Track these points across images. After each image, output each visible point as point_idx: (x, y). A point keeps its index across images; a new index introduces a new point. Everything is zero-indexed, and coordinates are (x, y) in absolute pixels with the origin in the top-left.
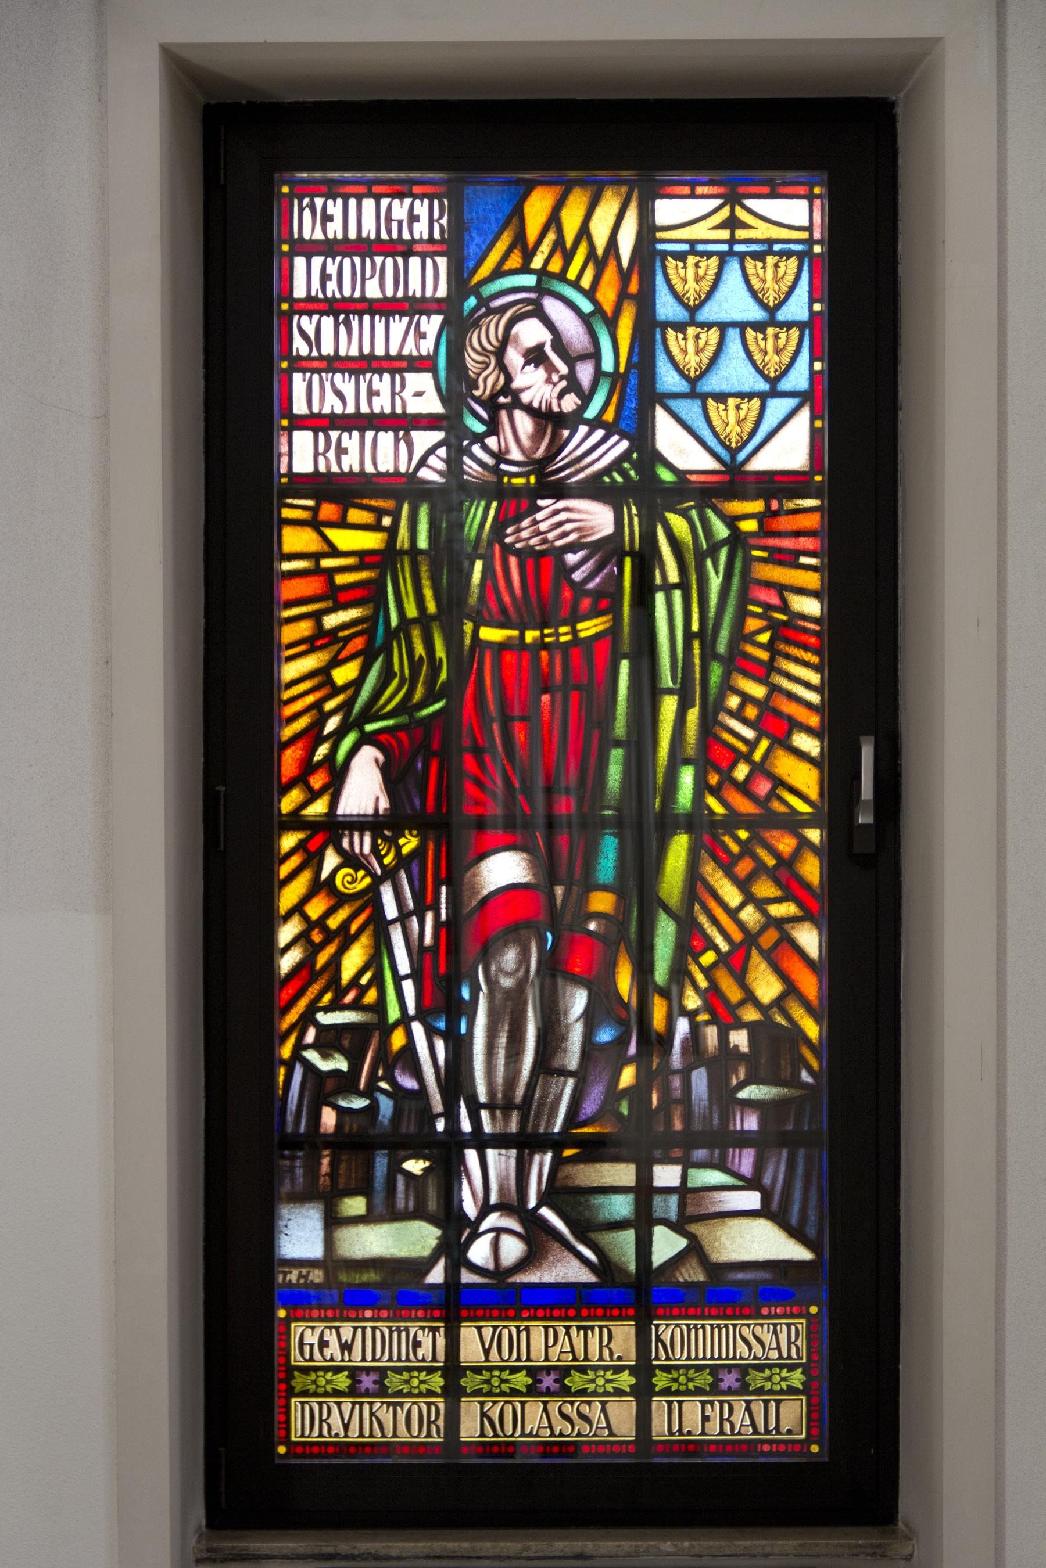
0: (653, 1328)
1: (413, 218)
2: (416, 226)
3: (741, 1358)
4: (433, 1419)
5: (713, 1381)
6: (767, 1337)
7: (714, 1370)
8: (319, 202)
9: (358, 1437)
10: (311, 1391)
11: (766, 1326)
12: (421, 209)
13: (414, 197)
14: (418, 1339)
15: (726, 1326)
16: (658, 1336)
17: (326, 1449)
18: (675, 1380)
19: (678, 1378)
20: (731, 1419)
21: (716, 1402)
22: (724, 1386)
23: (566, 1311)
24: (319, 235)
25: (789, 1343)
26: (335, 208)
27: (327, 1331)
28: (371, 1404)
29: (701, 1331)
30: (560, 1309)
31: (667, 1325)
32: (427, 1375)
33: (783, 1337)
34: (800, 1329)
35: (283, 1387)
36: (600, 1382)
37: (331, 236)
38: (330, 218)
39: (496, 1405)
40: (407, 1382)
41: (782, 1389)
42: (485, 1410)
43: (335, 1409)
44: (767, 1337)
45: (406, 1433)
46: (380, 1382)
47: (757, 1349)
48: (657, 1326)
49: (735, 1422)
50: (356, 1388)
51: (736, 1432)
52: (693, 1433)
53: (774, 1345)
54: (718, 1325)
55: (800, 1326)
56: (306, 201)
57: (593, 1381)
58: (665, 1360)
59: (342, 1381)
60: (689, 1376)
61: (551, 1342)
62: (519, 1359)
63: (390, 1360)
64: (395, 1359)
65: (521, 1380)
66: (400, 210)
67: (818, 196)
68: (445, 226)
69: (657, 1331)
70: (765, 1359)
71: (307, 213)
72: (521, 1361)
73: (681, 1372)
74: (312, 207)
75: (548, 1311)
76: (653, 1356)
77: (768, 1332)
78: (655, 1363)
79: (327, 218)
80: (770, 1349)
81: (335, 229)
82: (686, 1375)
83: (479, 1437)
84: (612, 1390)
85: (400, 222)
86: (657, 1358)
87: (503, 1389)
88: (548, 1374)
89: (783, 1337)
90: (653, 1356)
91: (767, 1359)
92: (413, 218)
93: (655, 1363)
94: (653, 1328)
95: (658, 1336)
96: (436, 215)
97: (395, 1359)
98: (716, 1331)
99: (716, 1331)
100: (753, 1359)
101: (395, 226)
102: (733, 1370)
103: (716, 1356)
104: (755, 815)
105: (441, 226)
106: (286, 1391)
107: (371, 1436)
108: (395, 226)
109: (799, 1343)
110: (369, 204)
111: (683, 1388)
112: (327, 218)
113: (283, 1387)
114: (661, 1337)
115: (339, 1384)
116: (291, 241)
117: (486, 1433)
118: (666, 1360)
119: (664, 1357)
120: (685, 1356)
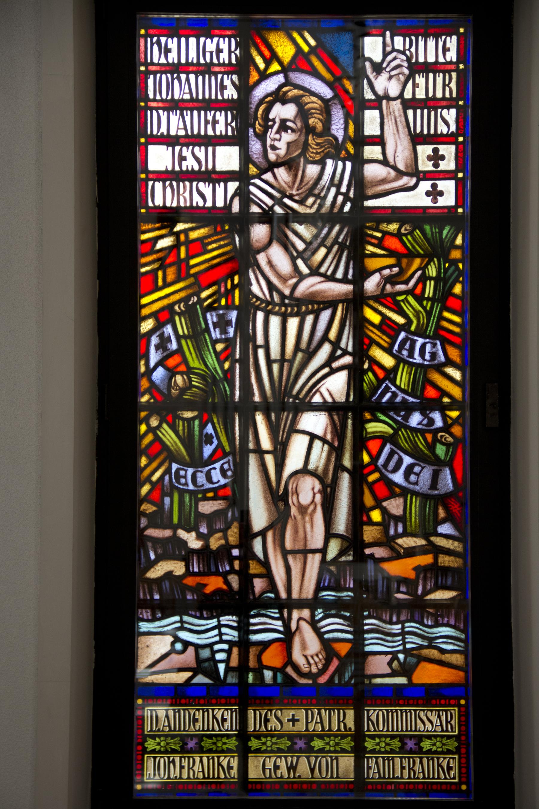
0: (366, 712)
1: (219, 51)
2: (221, 55)
3: (420, 731)
4: (191, 766)
5: (458, 746)
6: (434, 719)
7: (402, 738)
8: (163, 40)
9: (408, 779)
10: (157, 750)
11: (434, 712)
12: (224, 45)
13: (220, 36)
14: (225, 717)
15: (410, 711)
16: (368, 717)
17: (386, 787)
18: (387, 744)
19: (436, 743)
20: (194, 768)
21: (373, 758)
22: (297, 747)
23: (199, 701)
24: (163, 61)
25: (447, 722)
26: (172, 44)
27: (226, 712)
28: (438, 758)
29: (395, 714)
30: (436, 699)
31: (375, 710)
32: (390, 740)
33: (443, 718)
34: (454, 714)
35: (140, 748)
36: (269, 744)
37: (170, 61)
38: (170, 51)
39: (226, 758)
40: (215, 744)
41: (442, 751)
42: (440, 762)
43: (198, 759)
44: (434, 719)
45: (319, 774)
46: (199, 744)
47: (429, 726)
48: (368, 711)
49: (195, 770)
50: (184, 747)
51: (416, 777)
52: (302, 777)
53: (439, 724)
54: (406, 711)
55: (453, 712)
56: (155, 39)
57: (264, 744)
58: (373, 731)
59: (317, 744)
60: (443, 742)
61: (310, 720)
62: (388, 731)
63: (388, 731)
64: (211, 729)
65: (317, 744)
66: (211, 46)
67: (142, 64)
68: (238, 54)
69: (368, 714)
70: (434, 732)
71: (155, 47)
72: (389, 732)
73: (332, 738)
74: (159, 43)
75: (447, 701)
76: (366, 729)
77: (435, 715)
78: (366, 733)
79: (168, 51)
80: (436, 726)
81: (173, 57)
82: (441, 742)
83: (408, 779)
84: (276, 749)
85: (211, 53)
86: (368, 730)
87: (387, 749)
88: (192, 740)
89: (443, 718)
90: (366, 729)
91: (435, 731)
92: (219, 51)
93: (366, 733)
94: (366, 712)
95: (368, 717)
96: (233, 48)
97: (211, 729)
98: (404, 714)
99: (404, 714)
100: (426, 732)
101: (208, 55)
102: (194, 738)
103: (206, 729)
104: (448, 402)
105: (236, 55)
106: (142, 751)
107: (439, 778)
108: (208, 55)
109: (453, 722)
110: (192, 41)
111: (332, 749)
112: (168, 51)
113: (140, 748)
114: (371, 718)
115: (152, 743)
116: (146, 64)
117: (441, 777)
118: (374, 731)
119: (373, 730)
120: (385, 729)
